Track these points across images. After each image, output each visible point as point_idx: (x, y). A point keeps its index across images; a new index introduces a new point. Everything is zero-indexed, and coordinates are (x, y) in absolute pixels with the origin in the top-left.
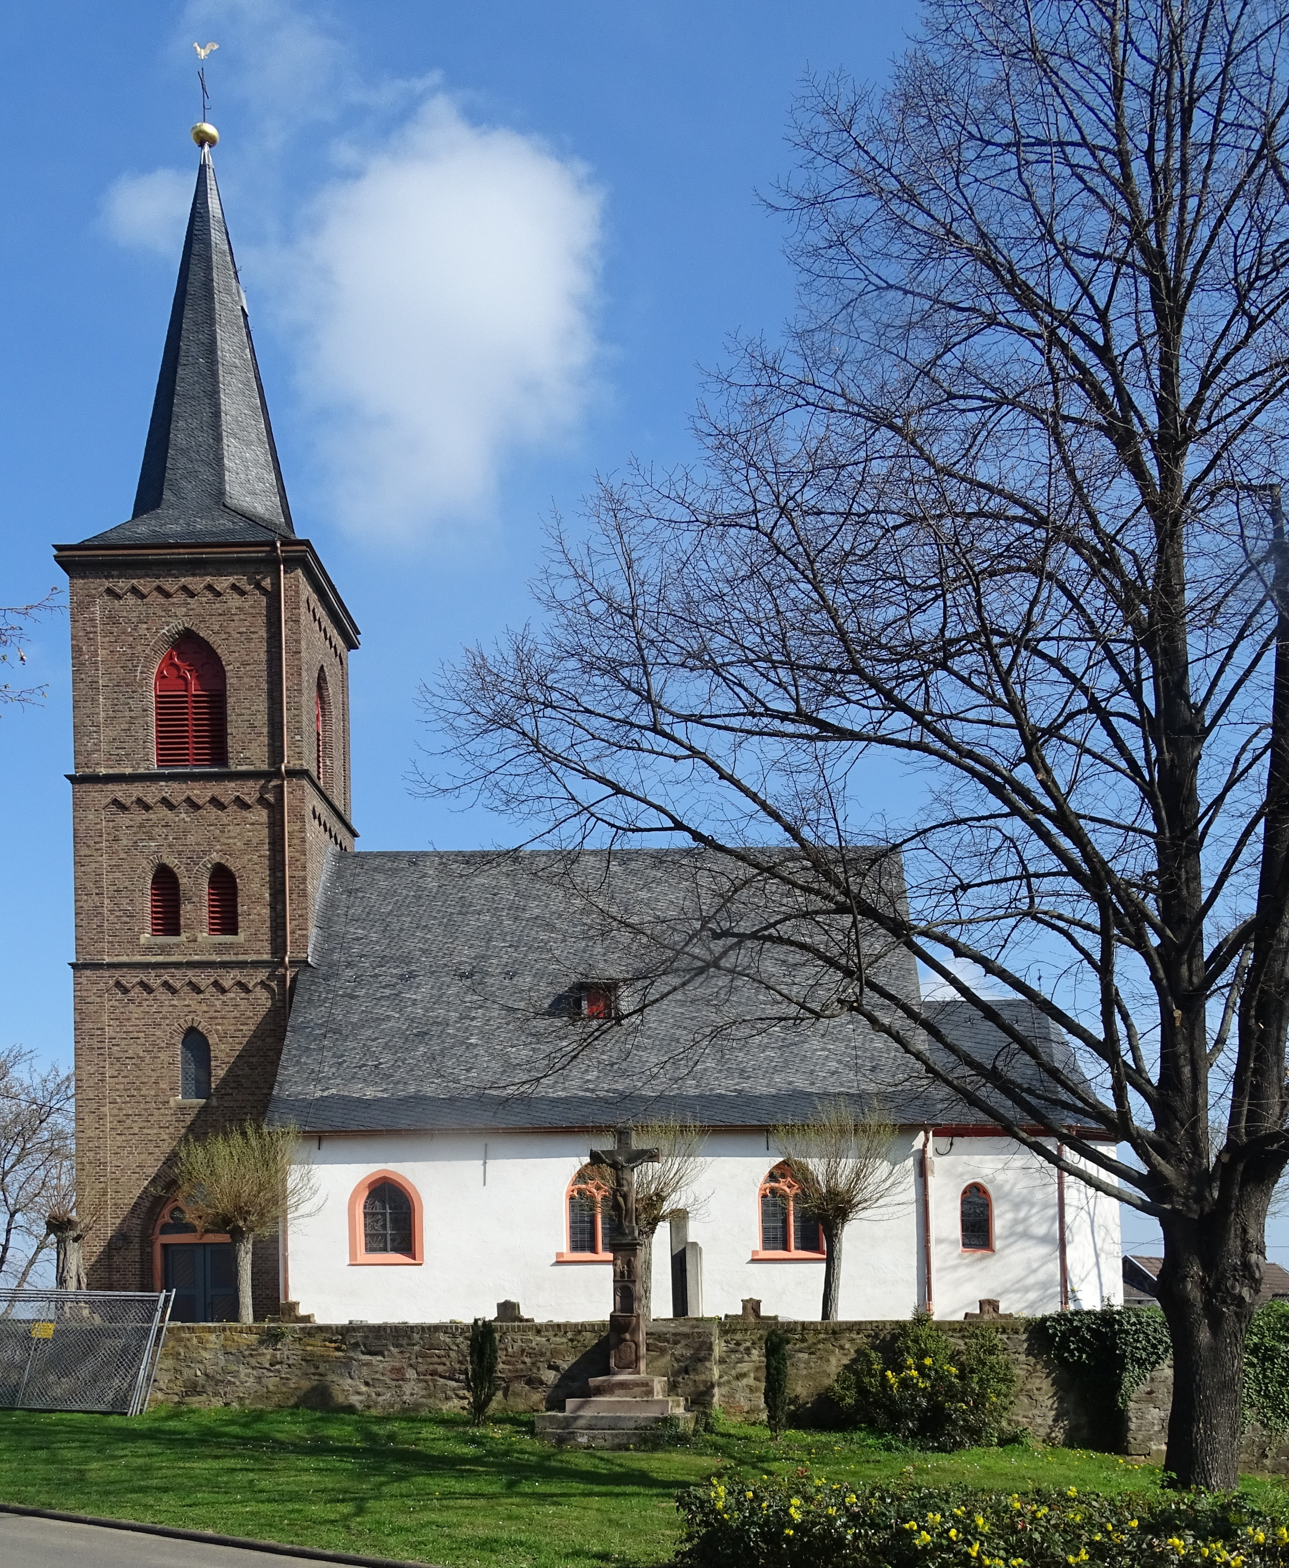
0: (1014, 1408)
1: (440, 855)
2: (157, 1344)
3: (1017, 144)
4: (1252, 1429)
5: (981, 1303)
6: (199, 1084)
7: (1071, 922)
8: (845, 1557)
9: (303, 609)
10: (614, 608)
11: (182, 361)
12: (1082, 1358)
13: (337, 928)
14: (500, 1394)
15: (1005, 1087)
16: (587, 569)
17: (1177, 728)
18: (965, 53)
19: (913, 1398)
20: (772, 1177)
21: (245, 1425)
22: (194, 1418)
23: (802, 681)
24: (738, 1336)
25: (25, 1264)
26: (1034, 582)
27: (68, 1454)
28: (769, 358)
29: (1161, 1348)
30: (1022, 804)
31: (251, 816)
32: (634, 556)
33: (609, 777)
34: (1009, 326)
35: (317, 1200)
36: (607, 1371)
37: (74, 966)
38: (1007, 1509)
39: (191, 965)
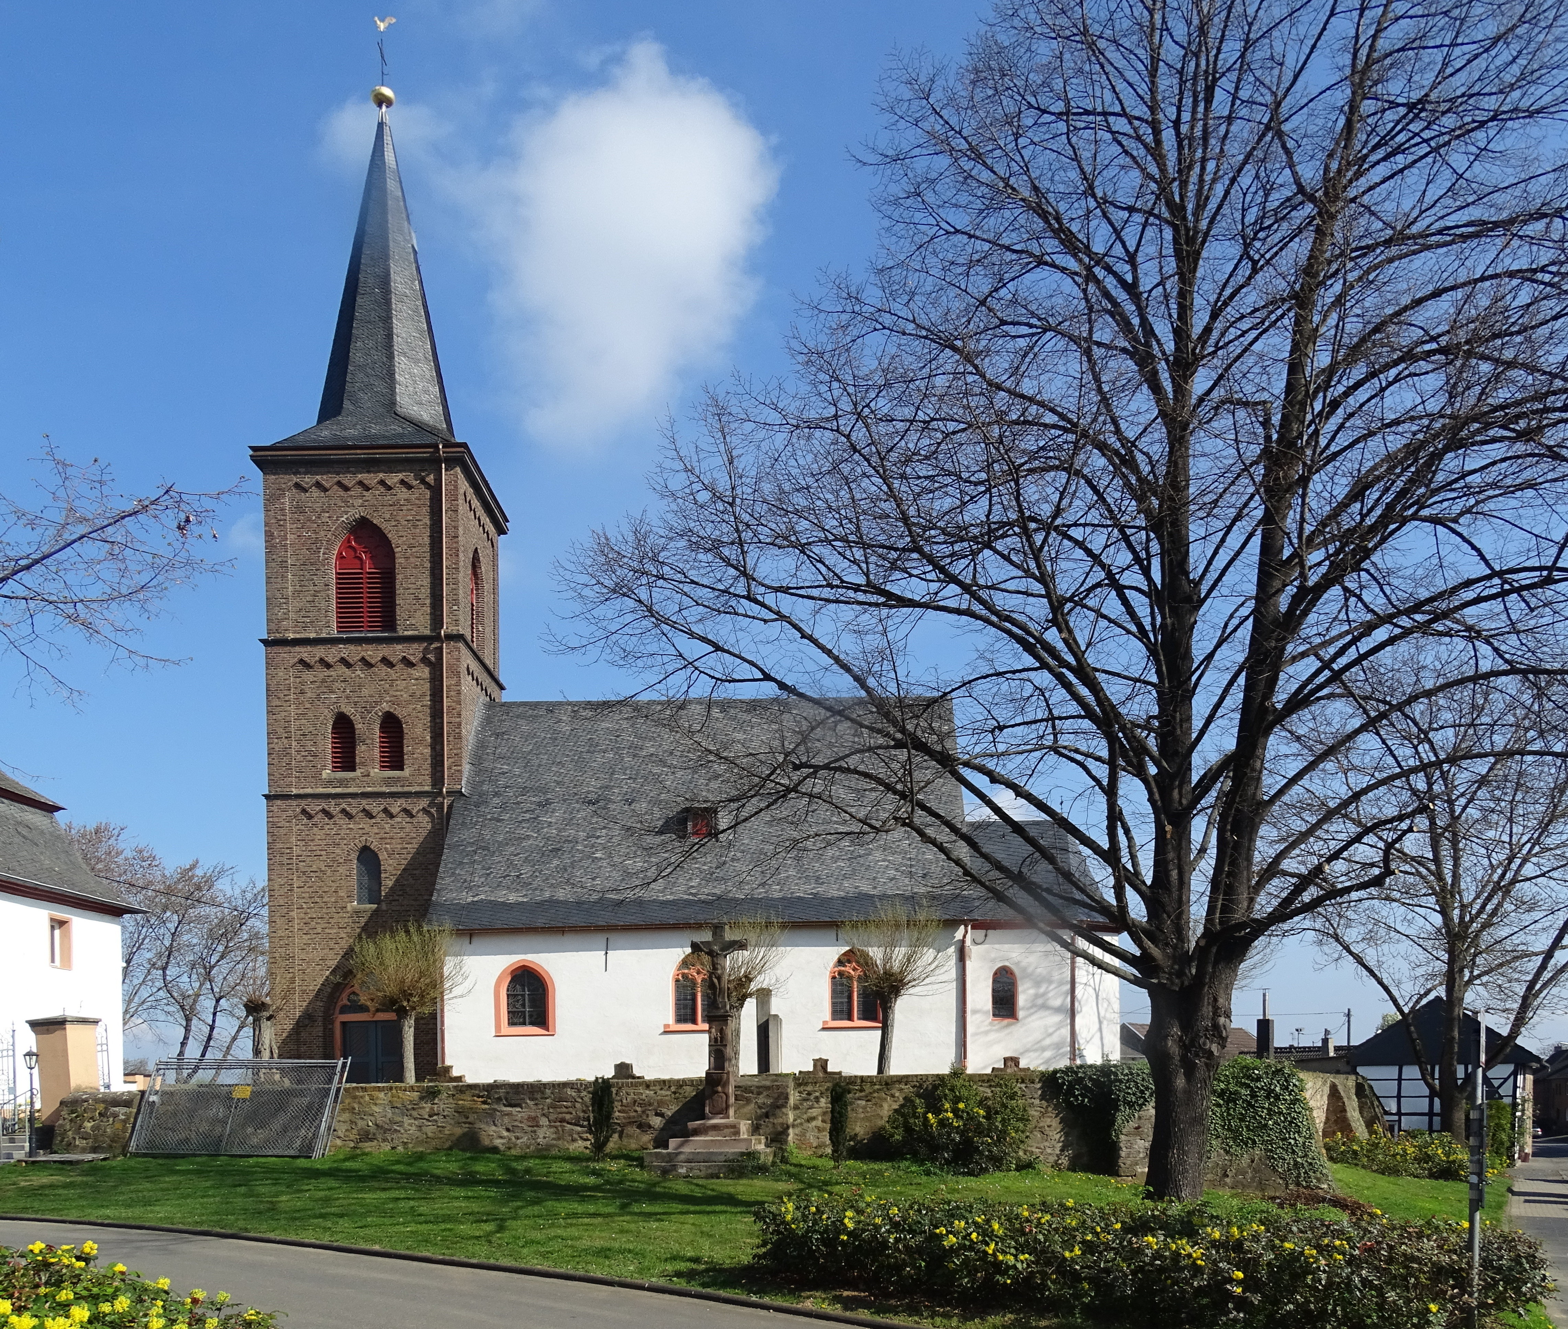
0: (1029, 1141)
2: (336, 1101)
3: (1067, 113)
4: (1217, 1156)
5: (1006, 1060)
7: (1087, 755)
8: (889, 1256)
9: (461, 501)
10: (717, 497)
11: (360, 291)
12: (1084, 1103)
13: (486, 764)
14: (616, 1136)
15: (1020, 881)
16: (695, 464)
17: (1178, 598)
18: (1028, 35)
19: (949, 1134)
20: (840, 962)
21: (409, 1164)
22: (367, 1159)
23: (873, 559)
24: (809, 1088)
25: (229, 1040)
26: (1064, 475)
27: (262, 1190)
28: (853, 289)
29: (1148, 1093)
30: (1050, 660)
31: (415, 673)
32: (734, 453)
34: (1053, 265)
35: (467, 984)
36: (703, 1117)
38: (1017, 1217)
39: (365, 795)
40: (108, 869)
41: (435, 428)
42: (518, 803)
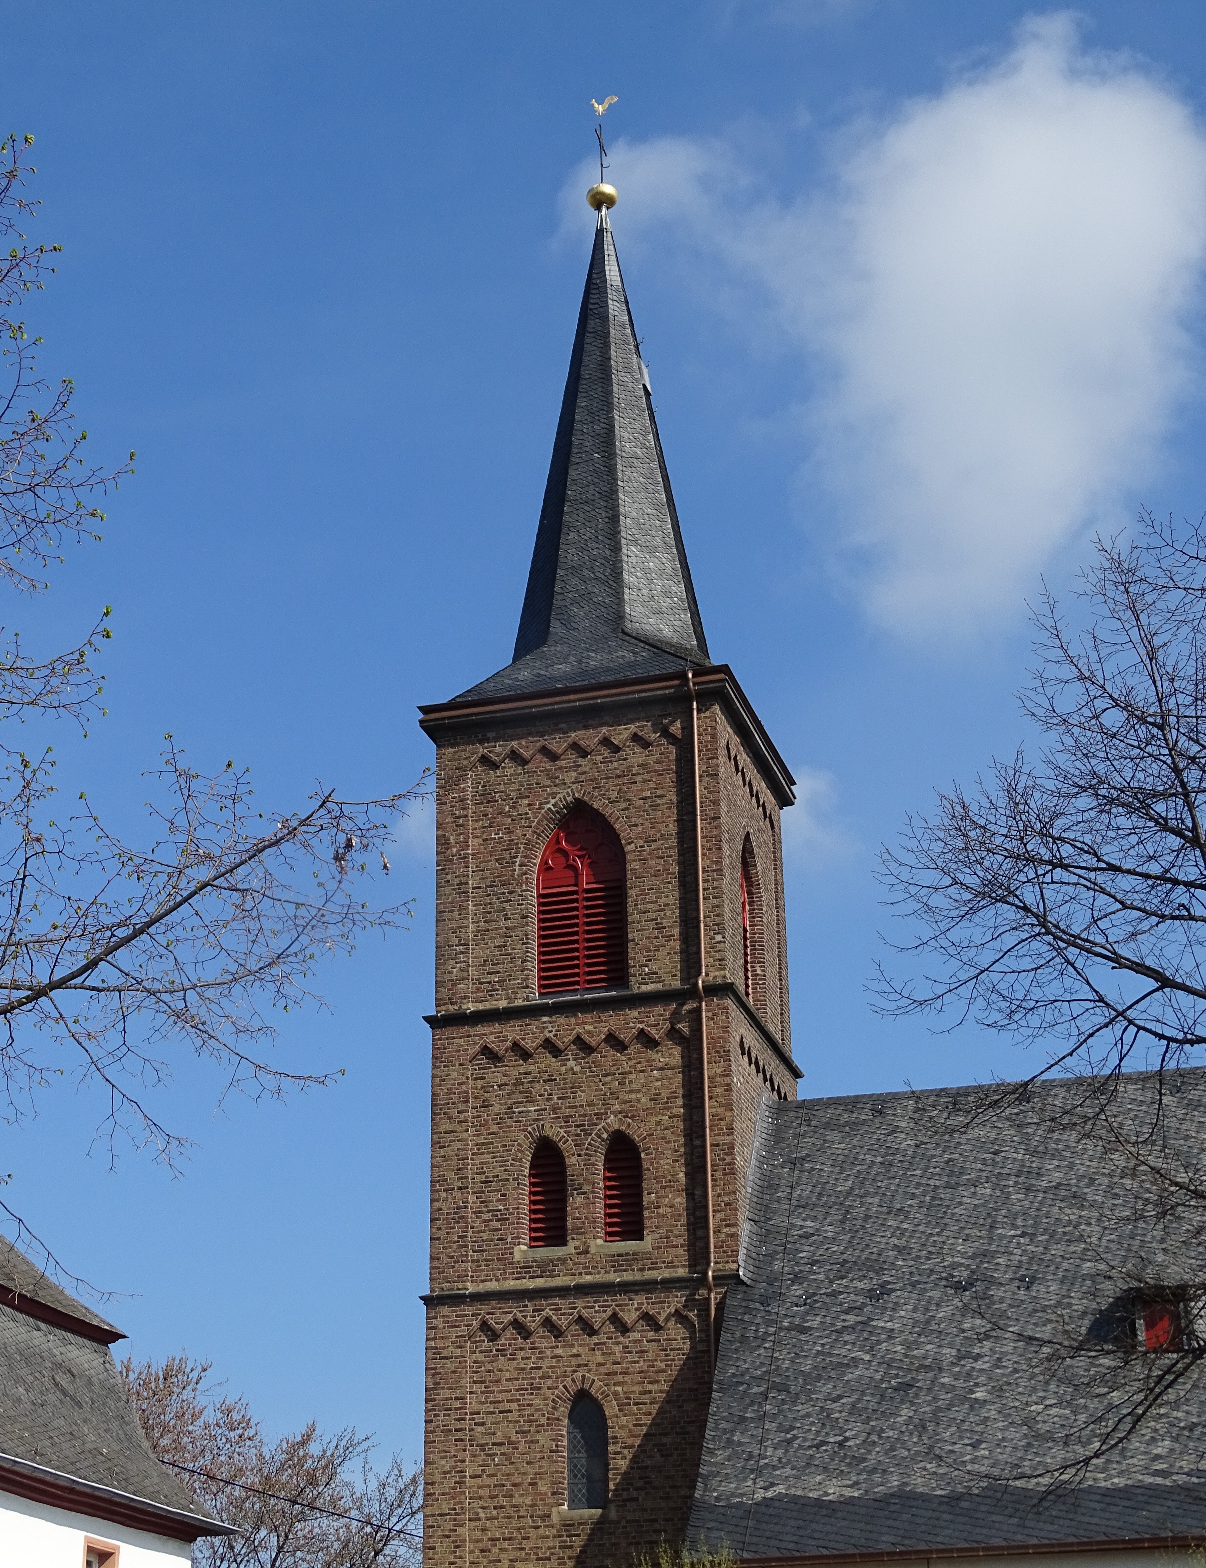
1: (915, 1096)
6: (591, 1486)
9: (722, 759)
13: (777, 1220)
16: (1095, 666)
32: (1157, 641)
33: (1149, 962)
37: (426, 1300)
39: (583, 1290)
40: (178, 1448)
41: (681, 647)
42: (835, 1294)
